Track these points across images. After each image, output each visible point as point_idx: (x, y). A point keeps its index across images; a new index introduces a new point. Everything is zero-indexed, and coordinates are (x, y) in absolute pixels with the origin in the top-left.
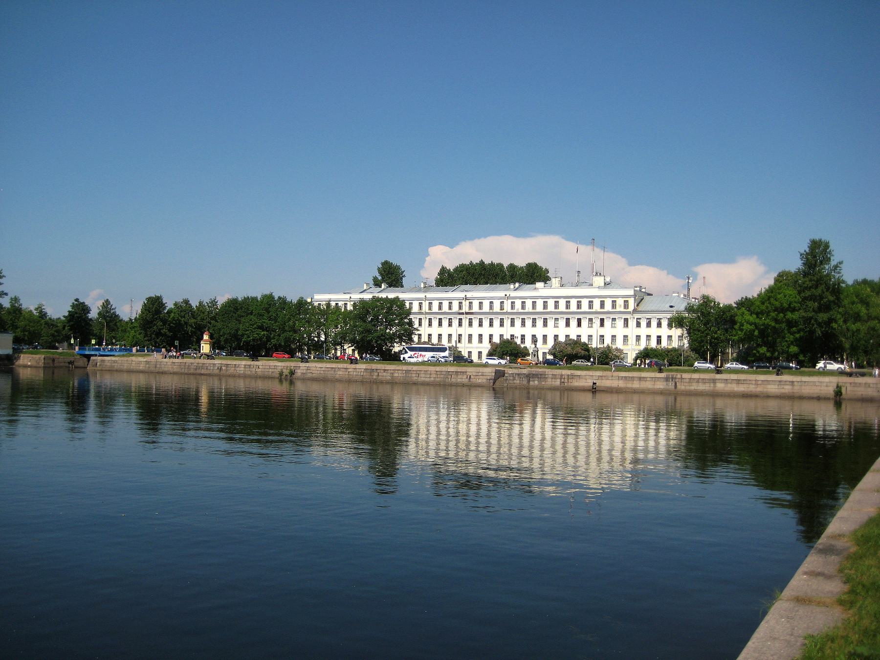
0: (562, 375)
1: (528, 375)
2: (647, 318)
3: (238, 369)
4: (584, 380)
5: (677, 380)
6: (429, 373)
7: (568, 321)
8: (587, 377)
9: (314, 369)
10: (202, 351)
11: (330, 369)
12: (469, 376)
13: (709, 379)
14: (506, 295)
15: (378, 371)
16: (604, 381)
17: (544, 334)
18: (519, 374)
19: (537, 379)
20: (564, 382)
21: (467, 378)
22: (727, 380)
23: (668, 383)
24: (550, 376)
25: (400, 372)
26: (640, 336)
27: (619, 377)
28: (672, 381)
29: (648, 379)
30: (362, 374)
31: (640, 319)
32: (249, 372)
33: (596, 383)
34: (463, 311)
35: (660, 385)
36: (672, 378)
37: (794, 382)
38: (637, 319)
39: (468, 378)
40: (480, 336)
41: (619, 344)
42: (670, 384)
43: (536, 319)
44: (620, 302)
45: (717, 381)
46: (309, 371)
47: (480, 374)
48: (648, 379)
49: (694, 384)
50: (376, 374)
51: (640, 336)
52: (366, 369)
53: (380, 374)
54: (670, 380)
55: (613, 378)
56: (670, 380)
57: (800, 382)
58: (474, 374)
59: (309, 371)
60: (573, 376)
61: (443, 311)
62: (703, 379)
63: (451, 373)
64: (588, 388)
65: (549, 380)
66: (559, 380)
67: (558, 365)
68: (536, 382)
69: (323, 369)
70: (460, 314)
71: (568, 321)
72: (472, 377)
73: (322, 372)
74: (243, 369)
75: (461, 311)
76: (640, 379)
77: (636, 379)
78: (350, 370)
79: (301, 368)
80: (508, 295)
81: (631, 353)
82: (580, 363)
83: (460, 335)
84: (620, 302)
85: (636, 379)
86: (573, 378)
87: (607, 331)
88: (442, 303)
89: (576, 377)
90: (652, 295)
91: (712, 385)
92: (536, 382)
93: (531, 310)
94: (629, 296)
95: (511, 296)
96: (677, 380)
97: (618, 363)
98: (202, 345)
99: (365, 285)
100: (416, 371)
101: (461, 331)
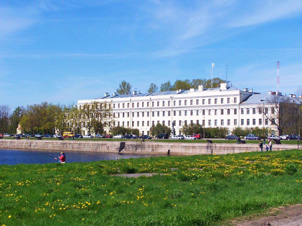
0: (153, 146)
1: (136, 145)
2: (247, 108)
3: (13, 144)
4: (164, 149)
5: (213, 148)
6: (89, 145)
7: (222, 111)
8: (166, 147)
9: (39, 143)
10: (17, 134)
11: (45, 143)
12: (108, 147)
13: (231, 147)
14: (171, 97)
15: (67, 144)
16: (174, 149)
17: (158, 120)
18: (131, 145)
19: (140, 148)
20: (153, 150)
21: (107, 148)
22: (240, 147)
23: (208, 149)
24: (147, 146)
25: (76, 144)
26: (124, 122)
27: (182, 146)
28: (210, 148)
29: (197, 148)
30: (59, 146)
31: (243, 109)
32: (12, 146)
33: (170, 150)
34: (170, 106)
35: (27, 145)
36: (210, 147)
37: (279, 148)
38: (242, 109)
39: (107, 147)
40: (254, 120)
41: (225, 125)
42: (209, 151)
43: (204, 110)
44: (232, 99)
45: (235, 148)
46: (37, 145)
47: (113, 145)
48: (197, 148)
49: (222, 150)
50: (65, 146)
51: (124, 122)
52: (61, 143)
53: (67, 146)
54: (209, 148)
55: (179, 147)
56: (209, 148)
57: (283, 148)
58: (110, 145)
59: (37, 145)
60: (158, 146)
61: (134, 108)
62: (227, 147)
63: (99, 145)
64: (165, 154)
65: (146, 148)
66: (151, 149)
67: (235, 139)
68: (140, 150)
69: (43, 143)
70: (174, 108)
71: (222, 111)
72: (109, 147)
73: (42, 145)
74: (9, 144)
75: (148, 107)
76: (193, 147)
77: (191, 147)
78: (54, 144)
79: (33, 143)
80: (172, 97)
81: (145, 130)
82: (272, 137)
83: (222, 120)
84: (232, 99)
85: (191, 147)
86: (158, 147)
87: (207, 117)
88: (119, 104)
89: (160, 147)
90: (260, 94)
91: (232, 151)
92: (140, 150)
93: (162, 107)
94: (237, 95)
95: (173, 97)
96: (213, 148)
97: (272, 137)
98: (17, 131)
99: (105, 94)
100: (84, 144)
101: (229, 117)
